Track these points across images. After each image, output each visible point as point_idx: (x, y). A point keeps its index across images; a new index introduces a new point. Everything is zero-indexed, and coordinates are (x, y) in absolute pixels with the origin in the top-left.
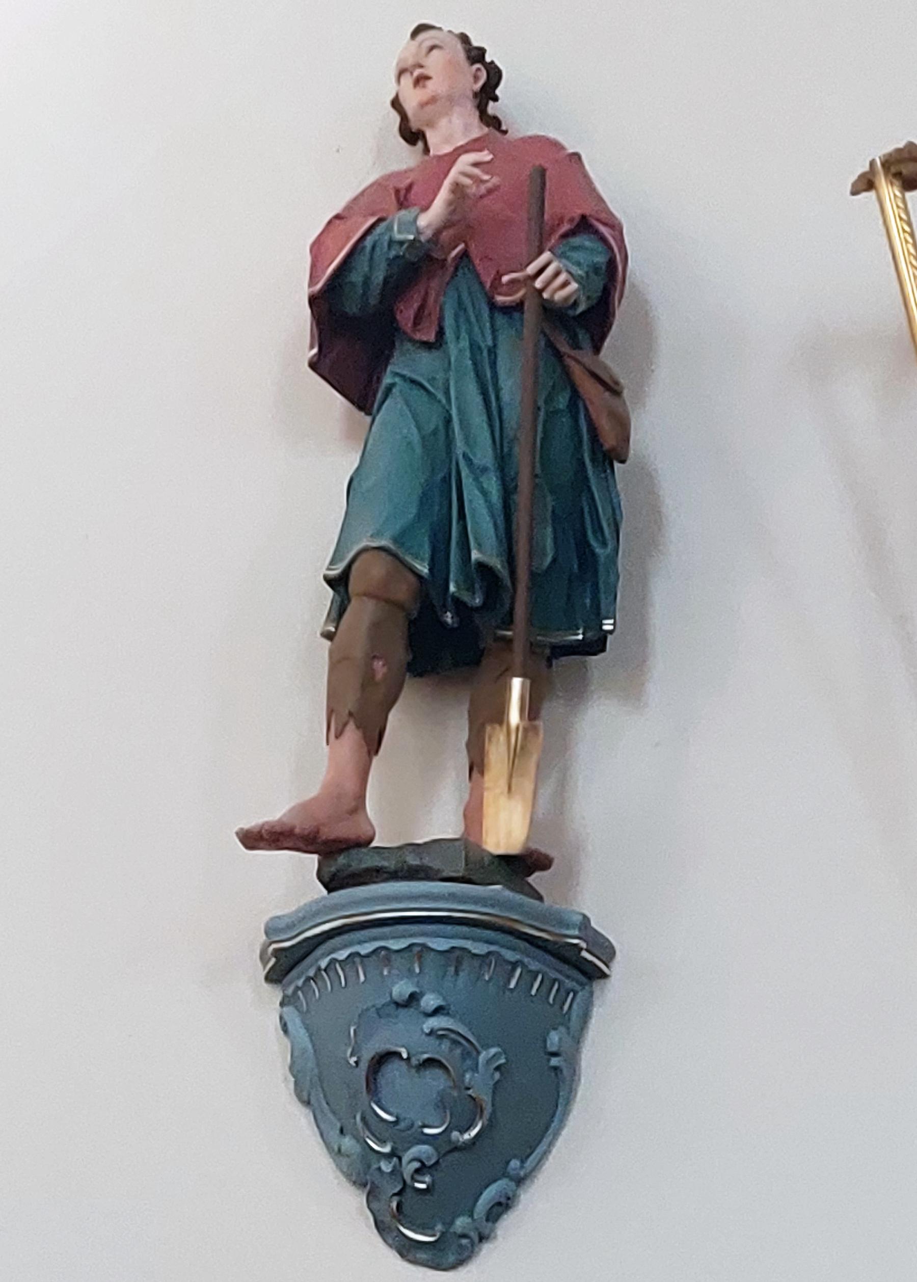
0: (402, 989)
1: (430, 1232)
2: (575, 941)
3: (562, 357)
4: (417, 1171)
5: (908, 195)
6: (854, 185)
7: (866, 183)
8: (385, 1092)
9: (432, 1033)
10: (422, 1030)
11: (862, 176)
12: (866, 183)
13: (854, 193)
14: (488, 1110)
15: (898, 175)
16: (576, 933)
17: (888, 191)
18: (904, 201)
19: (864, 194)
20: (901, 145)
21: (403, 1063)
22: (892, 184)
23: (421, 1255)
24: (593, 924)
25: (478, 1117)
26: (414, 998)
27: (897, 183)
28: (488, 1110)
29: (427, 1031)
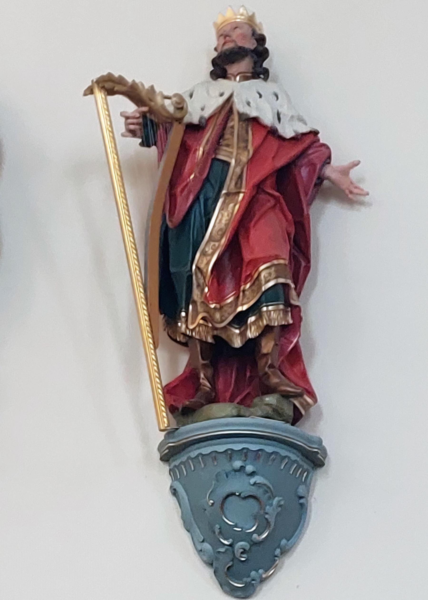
0: (238, 464)
1: (241, 582)
2: (316, 450)
3: (281, 210)
4: (242, 553)
5: (109, 98)
6: (85, 91)
7: (90, 91)
8: (227, 512)
9: (255, 484)
10: (250, 483)
11: (89, 88)
12: (90, 91)
13: (85, 95)
14: (272, 524)
15: (103, 88)
16: (316, 446)
17: (99, 95)
18: (106, 99)
19: (89, 96)
20: (105, 74)
21: (237, 498)
22: (101, 92)
23: (239, 593)
24: (323, 444)
25: (267, 528)
26: (242, 468)
27: (103, 91)
28: (272, 524)
29: (252, 483)
